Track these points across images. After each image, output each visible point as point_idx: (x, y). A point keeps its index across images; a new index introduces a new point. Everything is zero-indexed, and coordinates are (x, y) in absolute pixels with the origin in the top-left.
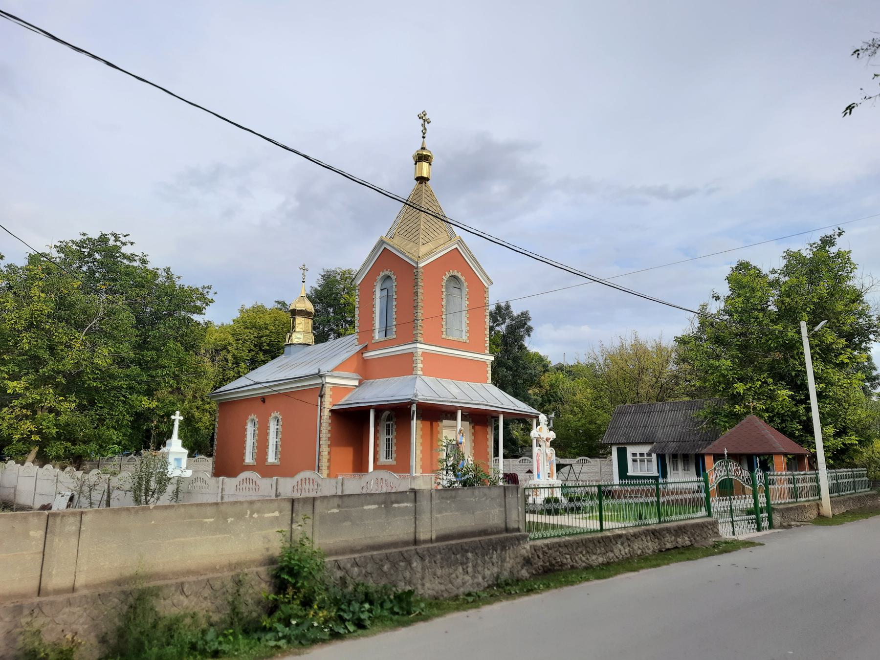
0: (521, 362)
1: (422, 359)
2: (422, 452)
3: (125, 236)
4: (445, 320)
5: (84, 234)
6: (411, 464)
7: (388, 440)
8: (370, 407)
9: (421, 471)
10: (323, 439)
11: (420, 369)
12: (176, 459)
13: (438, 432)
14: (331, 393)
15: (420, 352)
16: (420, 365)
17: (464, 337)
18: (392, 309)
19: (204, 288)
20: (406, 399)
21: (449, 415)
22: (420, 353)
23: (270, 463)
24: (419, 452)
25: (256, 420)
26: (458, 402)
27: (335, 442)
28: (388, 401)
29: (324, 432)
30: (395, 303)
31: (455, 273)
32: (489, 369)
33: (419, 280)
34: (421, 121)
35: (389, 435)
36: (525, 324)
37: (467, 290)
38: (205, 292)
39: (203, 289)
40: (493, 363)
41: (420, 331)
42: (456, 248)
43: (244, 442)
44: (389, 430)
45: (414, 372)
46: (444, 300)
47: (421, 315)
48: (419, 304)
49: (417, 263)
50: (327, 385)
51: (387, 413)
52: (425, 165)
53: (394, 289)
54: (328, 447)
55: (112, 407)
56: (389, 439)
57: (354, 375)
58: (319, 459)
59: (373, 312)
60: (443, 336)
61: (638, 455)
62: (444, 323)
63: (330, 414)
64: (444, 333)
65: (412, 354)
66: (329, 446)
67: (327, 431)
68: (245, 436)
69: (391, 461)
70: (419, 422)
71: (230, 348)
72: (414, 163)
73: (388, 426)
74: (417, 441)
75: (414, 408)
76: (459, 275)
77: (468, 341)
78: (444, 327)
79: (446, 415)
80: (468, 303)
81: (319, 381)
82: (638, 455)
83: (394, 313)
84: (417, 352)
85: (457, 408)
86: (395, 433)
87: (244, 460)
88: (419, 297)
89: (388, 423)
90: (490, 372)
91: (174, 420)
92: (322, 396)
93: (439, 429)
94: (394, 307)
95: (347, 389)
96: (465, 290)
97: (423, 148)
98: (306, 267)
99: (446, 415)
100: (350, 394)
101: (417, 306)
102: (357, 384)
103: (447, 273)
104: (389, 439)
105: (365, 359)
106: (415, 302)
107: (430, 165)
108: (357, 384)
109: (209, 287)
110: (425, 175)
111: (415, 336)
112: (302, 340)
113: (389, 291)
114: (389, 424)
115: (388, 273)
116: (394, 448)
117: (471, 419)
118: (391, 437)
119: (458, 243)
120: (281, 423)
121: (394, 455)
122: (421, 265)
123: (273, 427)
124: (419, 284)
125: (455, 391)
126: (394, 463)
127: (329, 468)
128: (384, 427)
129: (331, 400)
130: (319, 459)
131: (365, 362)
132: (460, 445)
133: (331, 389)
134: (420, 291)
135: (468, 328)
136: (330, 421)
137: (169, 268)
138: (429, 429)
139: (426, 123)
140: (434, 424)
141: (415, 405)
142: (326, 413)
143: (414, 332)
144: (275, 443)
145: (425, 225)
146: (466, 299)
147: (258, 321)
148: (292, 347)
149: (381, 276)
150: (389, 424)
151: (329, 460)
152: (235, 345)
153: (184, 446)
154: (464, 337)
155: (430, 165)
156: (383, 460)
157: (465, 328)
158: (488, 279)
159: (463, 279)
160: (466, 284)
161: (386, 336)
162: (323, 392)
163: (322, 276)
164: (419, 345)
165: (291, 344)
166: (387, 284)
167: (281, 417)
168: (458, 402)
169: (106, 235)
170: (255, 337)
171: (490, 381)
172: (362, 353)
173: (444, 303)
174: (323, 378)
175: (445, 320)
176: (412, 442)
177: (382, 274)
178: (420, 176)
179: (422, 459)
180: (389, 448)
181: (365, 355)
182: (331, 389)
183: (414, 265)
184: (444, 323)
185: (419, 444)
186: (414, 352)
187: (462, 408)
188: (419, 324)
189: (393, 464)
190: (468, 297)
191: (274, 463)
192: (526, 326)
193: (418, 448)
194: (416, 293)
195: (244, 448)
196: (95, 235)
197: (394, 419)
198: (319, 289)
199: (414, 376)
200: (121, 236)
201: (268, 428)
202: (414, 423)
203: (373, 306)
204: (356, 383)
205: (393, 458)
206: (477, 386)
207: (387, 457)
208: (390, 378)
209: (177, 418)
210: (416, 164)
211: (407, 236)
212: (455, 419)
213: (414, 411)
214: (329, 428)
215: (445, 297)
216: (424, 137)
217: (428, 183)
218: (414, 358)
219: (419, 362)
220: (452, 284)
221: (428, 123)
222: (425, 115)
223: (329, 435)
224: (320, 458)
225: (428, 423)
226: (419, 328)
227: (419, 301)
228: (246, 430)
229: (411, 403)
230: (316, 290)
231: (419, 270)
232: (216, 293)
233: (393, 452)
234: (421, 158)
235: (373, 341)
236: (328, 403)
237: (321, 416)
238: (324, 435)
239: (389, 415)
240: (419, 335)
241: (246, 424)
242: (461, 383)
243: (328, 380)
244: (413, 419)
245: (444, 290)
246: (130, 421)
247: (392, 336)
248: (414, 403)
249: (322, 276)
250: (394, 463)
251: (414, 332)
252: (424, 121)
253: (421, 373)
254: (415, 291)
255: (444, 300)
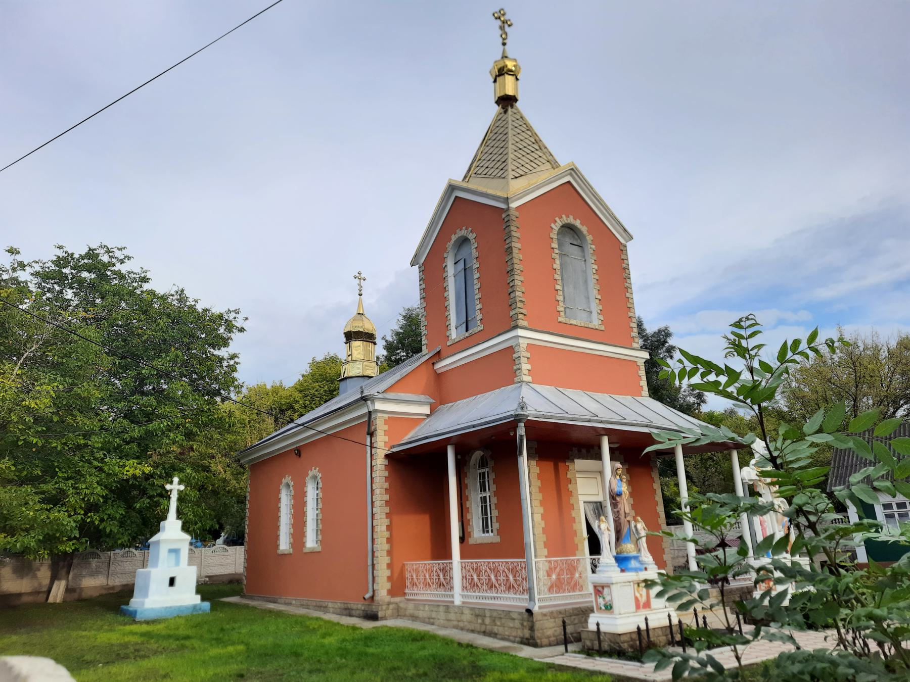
0: (665, 392)
1: (528, 355)
2: (543, 517)
3: (120, 249)
4: (561, 293)
5: (60, 247)
6: (526, 540)
7: (484, 500)
8: (448, 441)
9: (545, 552)
10: (377, 504)
11: (526, 372)
12: (171, 551)
13: (569, 481)
14: (386, 428)
15: (523, 343)
16: (525, 366)
17: (596, 322)
18: (473, 285)
19: (229, 312)
20: (506, 418)
21: (584, 451)
22: (525, 346)
23: (310, 548)
24: (538, 517)
25: (292, 483)
26: (601, 422)
27: (395, 507)
28: (474, 426)
29: (377, 491)
30: (477, 275)
31: (571, 220)
32: (642, 372)
33: (512, 228)
34: (499, 23)
35: (485, 490)
36: (665, 342)
37: (593, 247)
38: (231, 318)
39: (228, 313)
40: (647, 362)
41: (521, 310)
42: (569, 182)
43: (277, 518)
44: (484, 482)
45: (516, 379)
46: (558, 262)
47: (520, 284)
48: (516, 266)
49: (506, 200)
50: (379, 415)
51: (477, 455)
52: (509, 79)
53: (475, 254)
54: (387, 517)
55: (78, 476)
56: (485, 497)
57: (422, 398)
58: (373, 539)
59: (446, 299)
60: (560, 319)
61: (895, 507)
62: (560, 298)
63: (386, 462)
64: (562, 314)
65: (511, 349)
66: (388, 515)
67: (383, 491)
68: (278, 509)
69: (491, 537)
70: (533, 463)
71: (296, 406)
72: (493, 80)
73: (482, 476)
74: (533, 498)
75: (521, 431)
76: (578, 223)
77: (603, 328)
78: (561, 304)
79: (579, 451)
80: (596, 267)
81: (364, 411)
82: (895, 507)
83: (477, 292)
84: (518, 345)
85: (598, 433)
86: (493, 487)
87: (277, 546)
88: (515, 255)
89: (483, 471)
90: (644, 378)
91: (171, 491)
92: (371, 434)
93: (569, 475)
94: (476, 282)
95: (413, 421)
96: (590, 248)
97: (504, 57)
98: (362, 276)
99: (579, 451)
100: (418, 428)
101: (512, 270)
102: (428, 412)
103: (557, 219)
104: (485, 497)
105: (439, 372)
106: (509, 263)
107: (517, 79)
108: (428, 412)
109: (237, 312)
110: (510, 92)
111: (513, 318)
112: (360, 371)
113: (467, 262)
114: (484, 473)
115: (462, 233)
116: (495, 513)
117: (622, 457)
118: (487, 494)
119: (571, 175)
120: (320, 485)
121: (496, 526)
122: (514, 205)
123: (311, 493)
124: (513, 234)
125: (593, 407)
126: (498, 539)
127: (389, 553)
128: (476, 479)
129: (386, 439)
130: (373, 539)
131: (439, 377)
132: (618, 499)
133: (386, 422)
134: (516, 245)
135: (601, 307)
136: (387, 474)
137: (182, 291)
138: (553, 472)
139: (506, 26)
140: (561, 465)
141: (522, 425)
142: (380, 461)
143: (512, 313)
144: (315, 517)
145: (515, 163)
146: (593, 261)
147: (329, 371)
148: (348, 380)
149: (452, 242)
150: (484, 473)
151: (389, 540)
152: (301, 402)
153: (185, 528)
154: (596, 322)
155: (517, 79)
156: (477, 535)
157: (595, 307)
158: (625, 230)
159: (584, 229)
160: (589, 238)
161: (467, 330)
162: (373, 428)
163: (404, 316)
164: (520, 332)
165: (346, 378)
166: (464, 253)
167: (320, 475)
168: (601, 422)
169: (95, 250)
170: (325, 391)
171: (645, 391)
172: (433, 364)
173: (557, 266)
174: (369, 402)
175: (561, 293)
176: (523, 497)
177: (454, 238)
178: (502, 94)
179: (544, 531)
180: (486, 514)
181: (438, 366)
182: (386, 422)
183: (502, 206)
184: (560, 298)
185: (537, 503)
186: (514, 344)
187: (609, 432)
188: (518, 299)
189: (494, 541)
190: (595, 258)
191: (314, 548)
192: (667, 344)
193: (536, 510)
194: (509, 250)
195: (278, 528)
196: (79, 250)
197: (491, 463)
198: (401, 331)
199: (519, 385)
200: (115, 250)
201: (304, 494)
202: (524, 461)
203: (445, 289)
204: (427, 410)
205: (495, 532)
206: (627, 399)
207: (485, 529)
208: (479, 396)
209: (175, 487)
210: (495, 81)
211: (489, 173)
212: (598, 456)
213: (521, 436)
214: (386, 485)
215: (557, 256)
216: (504, 44)
217: (518, 104)
218: (515, 356)
219: (524, 360)
220: (568, 240)
221: (509, 26)
222: (503, 15)
223: (387, 497)
224: (375, 536)
225: (549, 465)
226: (519, 305)
227: (515, 261)
228: (279, 500)
229: (515, 421)
230: (398, 334)
231: (512, 212)
232: (247, 319)
233: (494, 520)
234: (502, 72)
235: (449, 344)
236: (383, 444)
237: (372, 467)
238: (379, 499)
239: (482, 458)
240: (521, 316)
241: (279, 492)
242: (598, 396)
243: (379, 406)
244: (521, 453)
245: (555, 245)
246: (102, 497)
247: (476, 328)
248: (520, 421)
249: (404, 316)
250: (498, 539)
251: (512, 313)
252: (503, 22)
253: (529, 379)
254: (507, 246)
255: (558, 262)
